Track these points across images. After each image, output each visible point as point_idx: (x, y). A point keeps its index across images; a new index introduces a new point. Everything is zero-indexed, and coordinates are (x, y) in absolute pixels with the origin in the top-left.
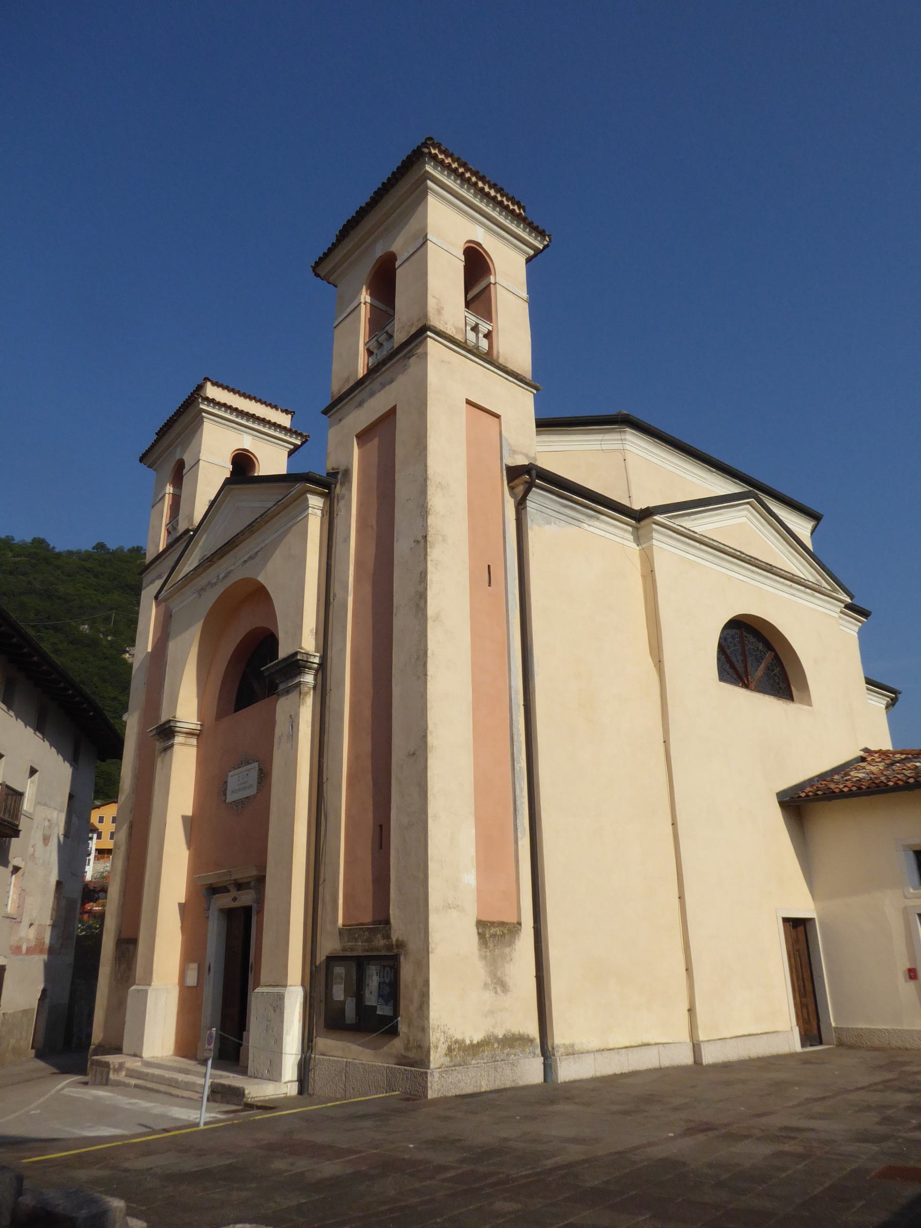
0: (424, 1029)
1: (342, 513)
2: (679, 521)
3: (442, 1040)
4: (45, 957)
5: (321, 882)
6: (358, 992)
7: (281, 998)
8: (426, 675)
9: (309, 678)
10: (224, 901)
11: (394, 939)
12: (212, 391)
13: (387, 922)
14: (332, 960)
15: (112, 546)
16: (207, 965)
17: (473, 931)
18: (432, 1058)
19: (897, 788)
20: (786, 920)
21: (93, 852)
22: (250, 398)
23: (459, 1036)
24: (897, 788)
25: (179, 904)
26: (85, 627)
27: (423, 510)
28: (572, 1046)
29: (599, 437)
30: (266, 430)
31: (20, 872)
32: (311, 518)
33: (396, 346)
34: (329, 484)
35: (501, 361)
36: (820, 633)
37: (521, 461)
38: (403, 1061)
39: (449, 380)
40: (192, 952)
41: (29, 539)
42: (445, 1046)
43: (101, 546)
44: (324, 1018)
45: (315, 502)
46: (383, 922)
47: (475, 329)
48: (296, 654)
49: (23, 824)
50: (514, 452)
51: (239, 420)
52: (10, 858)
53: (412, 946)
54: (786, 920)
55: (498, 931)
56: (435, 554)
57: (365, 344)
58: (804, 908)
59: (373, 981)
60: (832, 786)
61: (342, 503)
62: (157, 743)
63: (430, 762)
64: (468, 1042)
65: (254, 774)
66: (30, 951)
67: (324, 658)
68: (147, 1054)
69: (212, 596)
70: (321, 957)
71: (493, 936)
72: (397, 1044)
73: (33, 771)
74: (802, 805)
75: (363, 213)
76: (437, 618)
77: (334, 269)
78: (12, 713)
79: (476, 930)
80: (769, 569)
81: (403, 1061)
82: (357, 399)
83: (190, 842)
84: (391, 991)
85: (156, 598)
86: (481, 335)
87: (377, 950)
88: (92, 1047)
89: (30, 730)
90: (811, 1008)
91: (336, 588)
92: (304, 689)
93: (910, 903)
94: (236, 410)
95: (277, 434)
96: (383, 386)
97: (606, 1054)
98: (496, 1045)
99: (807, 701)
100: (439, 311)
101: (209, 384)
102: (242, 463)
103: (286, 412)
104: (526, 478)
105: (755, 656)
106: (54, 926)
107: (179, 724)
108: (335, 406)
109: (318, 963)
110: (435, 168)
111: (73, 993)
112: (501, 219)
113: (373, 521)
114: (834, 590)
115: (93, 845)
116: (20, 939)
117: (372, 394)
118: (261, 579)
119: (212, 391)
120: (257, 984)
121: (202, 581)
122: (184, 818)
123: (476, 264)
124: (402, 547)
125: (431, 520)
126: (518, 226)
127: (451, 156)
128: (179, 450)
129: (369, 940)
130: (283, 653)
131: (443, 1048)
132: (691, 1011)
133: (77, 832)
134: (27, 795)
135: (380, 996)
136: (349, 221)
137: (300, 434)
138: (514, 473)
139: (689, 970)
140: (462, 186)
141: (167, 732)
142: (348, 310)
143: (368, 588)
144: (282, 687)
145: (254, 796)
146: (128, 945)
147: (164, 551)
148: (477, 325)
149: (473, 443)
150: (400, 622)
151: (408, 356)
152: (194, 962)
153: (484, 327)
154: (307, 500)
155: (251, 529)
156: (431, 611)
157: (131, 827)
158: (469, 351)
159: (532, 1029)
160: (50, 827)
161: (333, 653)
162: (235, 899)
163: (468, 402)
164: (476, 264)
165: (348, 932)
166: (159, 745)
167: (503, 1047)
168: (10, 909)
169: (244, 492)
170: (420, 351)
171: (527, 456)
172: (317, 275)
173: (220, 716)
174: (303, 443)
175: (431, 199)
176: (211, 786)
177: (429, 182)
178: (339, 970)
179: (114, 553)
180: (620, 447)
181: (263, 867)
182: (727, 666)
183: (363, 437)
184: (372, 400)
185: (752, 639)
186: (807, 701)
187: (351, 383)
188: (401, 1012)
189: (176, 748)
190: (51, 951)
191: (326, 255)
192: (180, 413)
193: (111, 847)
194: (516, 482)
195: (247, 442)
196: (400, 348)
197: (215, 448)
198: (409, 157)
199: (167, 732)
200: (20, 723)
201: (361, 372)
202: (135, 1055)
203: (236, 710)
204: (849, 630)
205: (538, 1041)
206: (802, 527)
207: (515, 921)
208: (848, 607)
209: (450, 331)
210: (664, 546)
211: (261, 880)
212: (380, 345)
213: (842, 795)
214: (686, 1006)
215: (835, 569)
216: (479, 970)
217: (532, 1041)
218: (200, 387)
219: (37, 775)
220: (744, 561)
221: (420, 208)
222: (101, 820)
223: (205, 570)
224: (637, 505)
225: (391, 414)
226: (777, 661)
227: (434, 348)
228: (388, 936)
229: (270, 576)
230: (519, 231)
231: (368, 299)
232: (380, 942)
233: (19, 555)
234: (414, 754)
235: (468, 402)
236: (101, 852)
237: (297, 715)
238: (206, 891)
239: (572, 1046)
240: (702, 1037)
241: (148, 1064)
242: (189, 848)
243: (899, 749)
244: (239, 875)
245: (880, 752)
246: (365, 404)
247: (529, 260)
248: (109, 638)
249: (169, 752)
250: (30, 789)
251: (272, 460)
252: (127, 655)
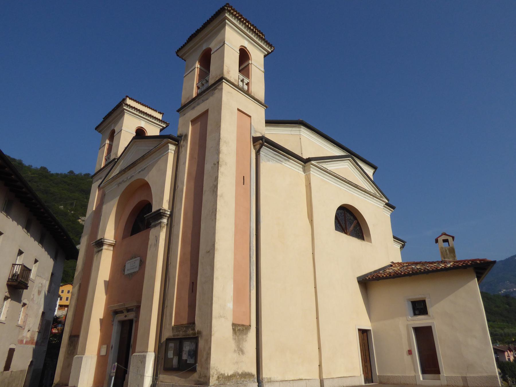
0: (208, 369)
1: (183, 153)
2: (321, 164)
3: (215, 373)
4: (34, 346)
5: (165, 306)
6: (179, 353)
7: (144, 357)
8: (216, 219)
9: (165, 221)
10: (121, 317)
11: (196, 331)
12: (129, 102)
13: (194, 323)
14: (168, 340)
15: (77, 172)
16: (111, 346)
17: (231, 327)
18: (210, 381)
19: (405, 275)
20: (359, 330)
21: (58, 306)
22: (145, 106)
23: (223, 372)
24: (405, 275)
25: (100, 319)
26: (62, 207)
27: (218, 152)
28: (270, 378)
29: (290, 129)
30: (151, 120)
31: (26, 306)
32: (170, 154)
33: (210, 85)
34: (178, 140)
35: (252, 94)
36: (375, 213)
37: (258, 135)
38: (198, 383)
39: (230, 100)
40: (104, 340)
41: (39, 167)
42: (217, 376)
43: (71, 172)
44: (163, 366)
45: (172, 148)
46: (192, 323)
47: (242, 81)
48: (160, 210)
49: (30, 284)
50: (256, 132)
51: (140, 115)
52: (22, 299)
53: (204, 333)
54: (359, 330)
55: (241, 328)
56: (222, 169)
57: (197, 84)
58: (367, 325)
59: (187, 347)
60: (379, 275)
61: (183, 149)
62: (95, 249)
63: (216, 255)
64: (226, 375)
65: (138, 263)
66: (27, 343)
67: (172, 212)
70: (163, 339)
71: (239, 330)
72: (195, 376)
73: (36, 261)
74: (366, 283)
75: (198, 32)
76: (221, 196)
77: (185, 54)
78: (29, 234)
79: (231, 327)
80: (356, 186)
81: (198, 383)
82: (193, 106)
83: (107, 292)
84: (194, 354)
85: (99, 186)
86: (245, 84)
87: (188, 335)
88: (54, 385)
89: (36, 243)
90: (369, 367)
91: (179, 183)
92: (163, 225)
93: (409, 323)
94: (139, 110)
95: (156, 122)
96: (203, 101)
97: (284, 382)
98: (238, 377)
99: (370, 241)
100: (228, 72)
101: (128, 99)
102: (140, 133)
103: (160, 113)
104: (260, 142)
105: (349, 221)
106: (39, 332)
107: (105, 241)
108: (182, 109)
109: (162, 342)
110: (229, 15)
111: (45, 365)
112: (255, 38)
113: (196, 156)
114: (381, 197)
115: (58, 302)
116: (23, 337)
117: (198, 104)
118: (146, 179)
119: (129, 102)
120: (134, 352)
121: (120, 180)
122: (105, 281)
123: (244, 56)
124: (208, 167)
125: (221, 156)
126: (261, 42)
127: (236, 11)
128: (113, 125)
129: (185, 331)
130: (154, 210)
131: (215, 377)
132: (320, 366)
133: (52, 295)
134: (32, 271)
135: (189, 355)
136: (192, 35)
137: (166, 123)
138: (255, 140)
139: (319, 348)
140: (240, 24)
141: (100, 244)
142: (190, 70)
143: (192, 184)
144: (153, 224)
146: (75, 338)
147: (104, 167)
148: (243, 79)
149: (240, 127)
150: (206, 197)
151: (215, 89)
152: (104, 344)
153: (246, 81)
154: (168, 146)
155: (143, 158)
156: (219, 192)
157: (80, 286)
158: (240, 89)
159: (253, 371)
160: (41, 287)
161: (176, 210)
162: (126, 316)
163: (238, 110)
164: (244, 56)
165: (177, 328)
166: (96, 250)
167: (241, 378)
168: (20, 322)
169: (141, 142)
170: (220, 87)
171: (261, 133)
172: (178, 55)
173: (124, 237)
174: (166, 127)
175: (227, 28)
176: (118, 267)
177: (227, 21)
178: (171, 345)
179: (77, 175)
180: (299, 133)
181: (139, 302)
182: (338, 225)
183: (194, 121)
184: (199, 106)
185: (349, 215)
186: (370, 241)
187: (190, 99)
188: (198, 362)
189: (103, 251)
190: (37, 344)
191: (182, 47)
192: (114, 110)
193: (68, 304)
194: (256, 143)
195: (143, 124)
196: (211, 86)
197: (129, 125)
198: (219, 10)
199: (100, 244)
200: (32, 239)
201: (194, 95)
203: (132, 235)
204: (387, 214)
205: (256, 376)
206: (370, 171)
207: (248, 324)
208: (387, 204)
209: (233, 80)
210: (315, 174)
211: (138, 307)
212: (203, 85)
213: (383, 278)
214: (318, 364)
215: (382, 188)
216: (232, 344)
217: (253, 376)
218: (124, 100)
219: (38, 263)
220: (345, 183)
221: (222, 31)
222: (62, 292)
223: (122, 175)
224: (305, 157)
225: (206, 112)
226: (358, 224)
227: (225, 86)
228: (194, 329)
229: (150, 178)
230: (262, 44)
231: (199, 66)
232: (190, 332)
233: (34, 174)
235: (238, 110)
236: (61, 306)
237: (159, 236)
238: (113, 313)
239: (270, 378)
240: (324, 377)
242: (106, 294)
243: (406, 262)
244: (128, 305)
245: (398, 263)
246: (195, 108)
247: (265, 56)
248: (72, 212)
249: (100, 253)
250: (34, 269)
251: (153, 130)
252: (80, 220)
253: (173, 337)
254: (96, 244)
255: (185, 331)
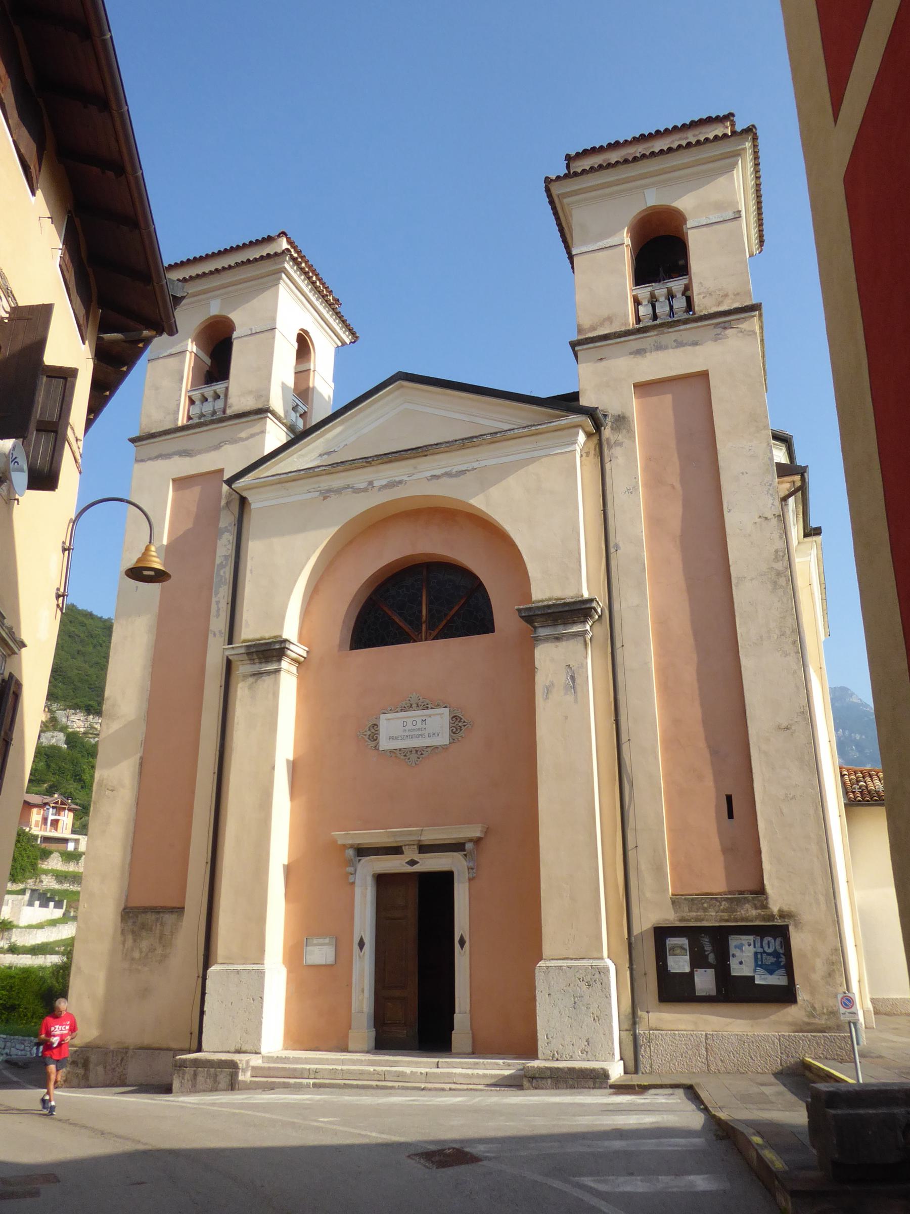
53: (810, 913)
57: (187, 391)
68: (264, 1050)
69: (358, 505)
96: (680, 344)
117: (659, 348)
145: (444, 748)
177: (283, 275)
202: (256, 1053)
212: (205, 399)
228: (765, 907)
231: (194, 349)
232: (749, 913)
234: (787, 728)
241: (269, 1059)
253: (678, 924)
254: (248, 654)
255: (730, 910)
